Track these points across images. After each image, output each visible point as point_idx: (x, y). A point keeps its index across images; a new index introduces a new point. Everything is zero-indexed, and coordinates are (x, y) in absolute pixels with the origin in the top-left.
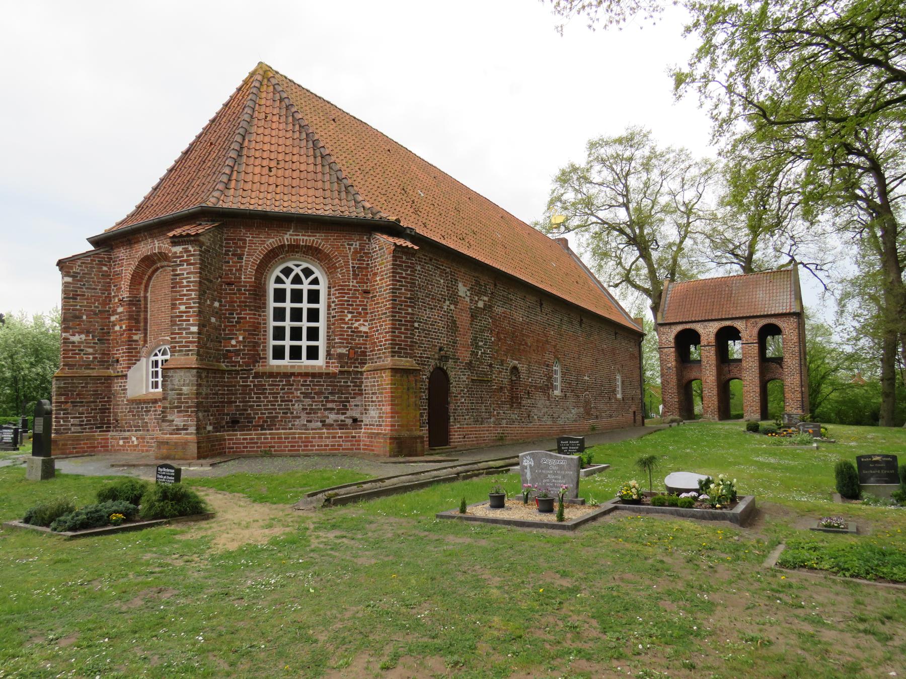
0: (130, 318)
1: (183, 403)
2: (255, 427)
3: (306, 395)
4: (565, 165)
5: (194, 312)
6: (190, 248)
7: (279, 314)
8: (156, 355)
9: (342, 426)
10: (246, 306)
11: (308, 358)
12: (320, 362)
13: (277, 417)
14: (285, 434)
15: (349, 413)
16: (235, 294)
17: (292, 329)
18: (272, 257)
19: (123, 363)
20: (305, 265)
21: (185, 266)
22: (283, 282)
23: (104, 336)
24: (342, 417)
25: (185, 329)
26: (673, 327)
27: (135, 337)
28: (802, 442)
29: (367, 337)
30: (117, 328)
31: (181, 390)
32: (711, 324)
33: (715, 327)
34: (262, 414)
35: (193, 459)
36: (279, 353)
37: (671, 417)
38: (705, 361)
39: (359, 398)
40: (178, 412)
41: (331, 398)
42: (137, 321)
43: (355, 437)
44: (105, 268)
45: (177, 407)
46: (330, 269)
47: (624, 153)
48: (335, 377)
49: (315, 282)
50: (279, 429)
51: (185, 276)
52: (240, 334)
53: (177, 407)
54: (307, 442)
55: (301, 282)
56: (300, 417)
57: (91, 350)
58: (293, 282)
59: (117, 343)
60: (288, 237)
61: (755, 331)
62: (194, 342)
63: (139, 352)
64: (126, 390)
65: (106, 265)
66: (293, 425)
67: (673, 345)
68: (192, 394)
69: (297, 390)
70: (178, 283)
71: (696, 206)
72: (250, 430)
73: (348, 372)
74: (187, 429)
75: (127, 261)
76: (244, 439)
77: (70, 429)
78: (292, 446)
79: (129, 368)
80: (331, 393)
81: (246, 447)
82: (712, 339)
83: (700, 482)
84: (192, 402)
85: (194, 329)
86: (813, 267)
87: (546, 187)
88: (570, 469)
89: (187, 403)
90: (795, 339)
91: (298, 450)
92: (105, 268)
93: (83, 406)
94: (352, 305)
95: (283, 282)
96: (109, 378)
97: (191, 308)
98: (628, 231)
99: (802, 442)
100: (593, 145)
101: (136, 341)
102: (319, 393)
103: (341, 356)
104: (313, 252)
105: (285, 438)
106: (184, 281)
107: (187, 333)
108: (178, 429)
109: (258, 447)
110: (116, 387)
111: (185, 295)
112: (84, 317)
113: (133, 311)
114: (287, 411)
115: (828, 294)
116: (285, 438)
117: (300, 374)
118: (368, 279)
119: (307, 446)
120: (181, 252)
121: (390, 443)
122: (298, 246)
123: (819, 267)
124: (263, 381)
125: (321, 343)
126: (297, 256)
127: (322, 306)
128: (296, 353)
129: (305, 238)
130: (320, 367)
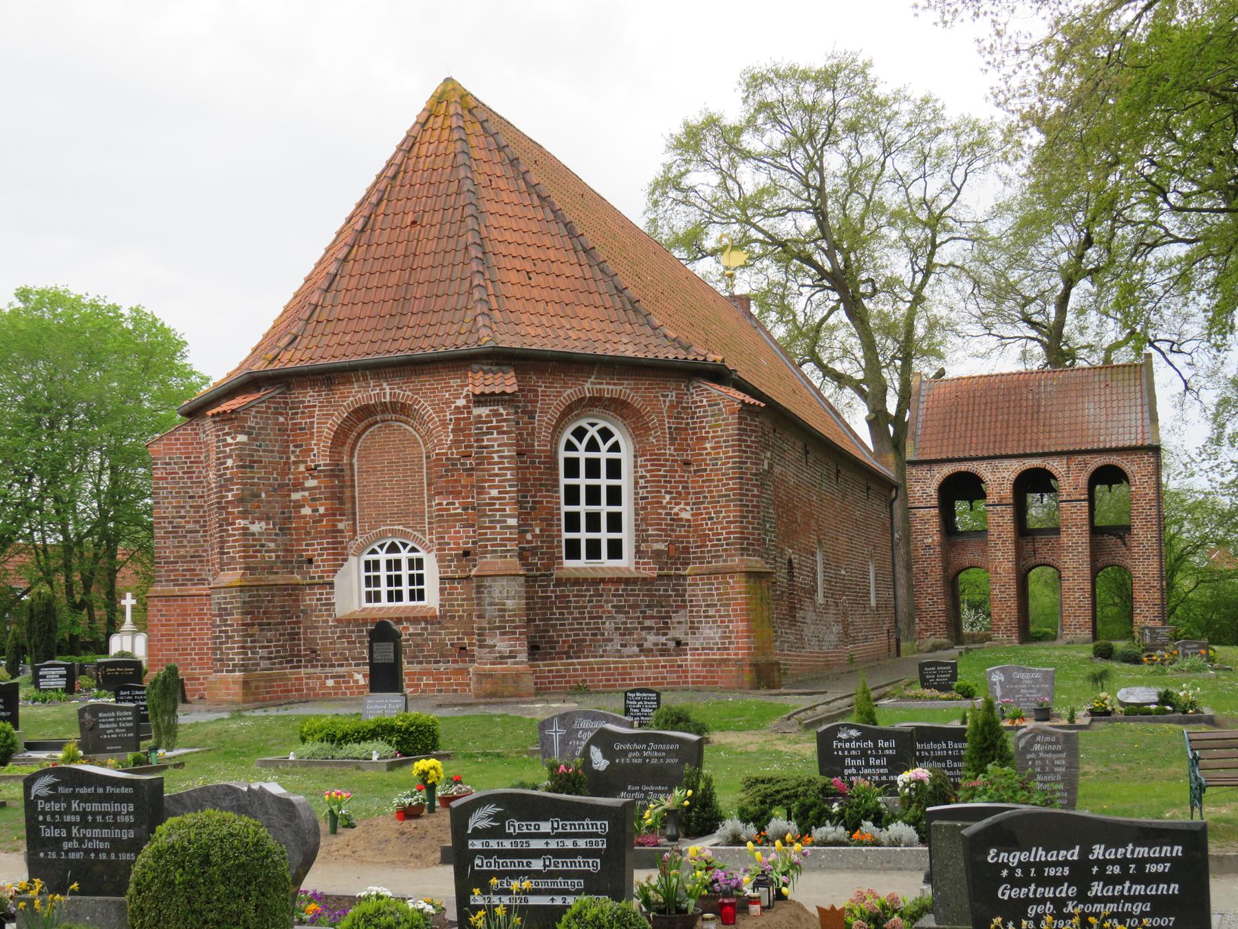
0: (333, 497)
1: (507, 622)
2: (560, 655)
3: (619, 609)
4: (696, 119)
5: (511, 498)
6: (501, 410)
7: (572, 495)
8: (374, 552)
9: (664, 651)
10: (541, 485)
11: (609, 557)
12: (627, 562)
13: (585, 640)
14: (596, 663)
15: (672, 634)
16: (527, 468)
17: (588, 515)
18: (569, 412)
19: (322, 562)
20: (602, 424)
21: (495, 435)
22: (576, 449)
23: (285, 522)
24: (663, 639)
25: (499, 522)
26: (936, 468)
27: (341, 526)
28: (1192, 669)
29: (689, 526)
30: (306, 511)
31: (504, 604)
32: (1006, 463)
33: (1012, 469)
34: (567, 636)
35: (530, 695)
36: (573, 550)
37: (932, 640)
38: (994, 531)
39: (682, 612)
40: (501, 634)
41: (649, 612)
42: (341, 501)
43: (680, 666)
44: (281, 419)
45: (499, 628)
46: (639, 430)
47: (820, 109)
48: (652, 584)
49: (615, 448)
50: (587, 657)
51: (496, 448)
52: (537, 525)
53: (499, 628)
54: (624, 673)
55: (597, 449)
56: (612, 640)
57: (272, 545)
58: (588, 449)
59: (308, 533)
60: (590, 386)
61: (1083, 480)
62: (514, 540)
63: (345, 548)
64: (333, 604)
65: (281, 414)
66: (604, 651)
67: (935, 502)
68: (520, 609)
69: (607, 602)
70: (485, 458)
71: (949, 212)
72: (553, 659)
73: (669, 576)
74: (515, 657)
75: (322, 414)
76: (550, 671)
77: (258, 665)
78: (607, 680)
79: (335, 571)
80: (650, 606)
81: (552, 682)
82: (1007, 491)
83: (1159, 695)
84: (520, 621)
85: (513, 522)
86: (1165, 347)
87: (655, 158)
88: (1045, 682)
89: (513, 621)
90: (1152, 496)
91: (614, 686)
92: (281, 419)
93: (270, 630)
94: (670, 482)
95: (576, 449)
96: (296, 586)
97: (507, 492)
98: (820, 258)
99: (1192, 669)
100: (755, 82)
101: (342, 531)
102: (634, 606)
103: (658, 554)
104: (618, 407)
105: (599, 669)
106: (495, 455)
107: (501, 528)
108: (502, 657)
109: (566, 682)
110: (310, 599)
111: (497, 475)
112: (263, 495)
113: (334, 487)
114: (597, 632)
115: (1189, 397)
116: (599, 669)
117: (611, 581)
118: (688, 445)
119: (624, 680)
120: (488, 416)
121: (751, 671)
122: (600, 399)
123: (1175, 348)
124: (567, 590)
125: (626, 535)
126: (596, 411)
127: (625, 482)
128: (594, 550)
129: (611, 387)
130: (628, 569)
